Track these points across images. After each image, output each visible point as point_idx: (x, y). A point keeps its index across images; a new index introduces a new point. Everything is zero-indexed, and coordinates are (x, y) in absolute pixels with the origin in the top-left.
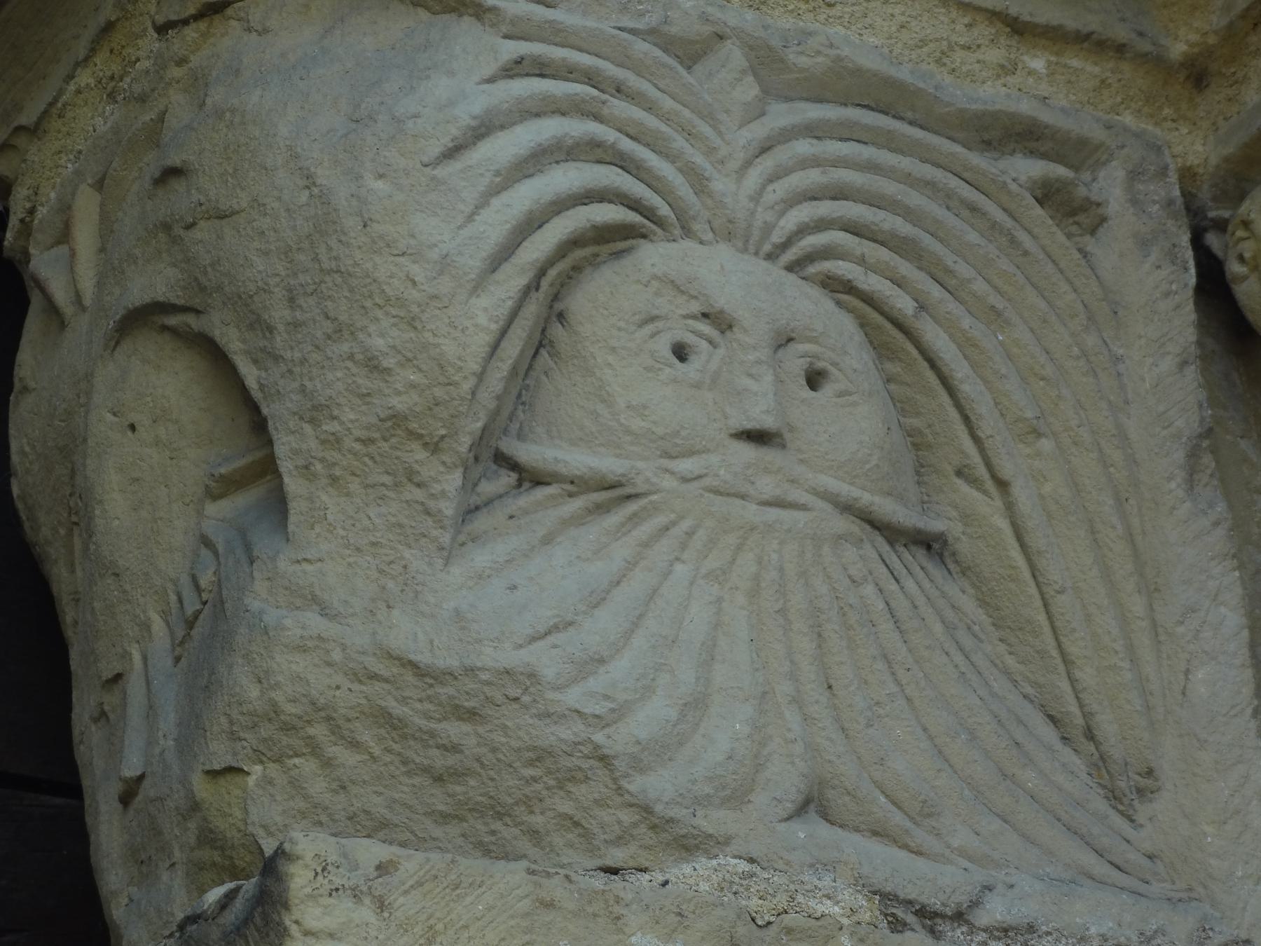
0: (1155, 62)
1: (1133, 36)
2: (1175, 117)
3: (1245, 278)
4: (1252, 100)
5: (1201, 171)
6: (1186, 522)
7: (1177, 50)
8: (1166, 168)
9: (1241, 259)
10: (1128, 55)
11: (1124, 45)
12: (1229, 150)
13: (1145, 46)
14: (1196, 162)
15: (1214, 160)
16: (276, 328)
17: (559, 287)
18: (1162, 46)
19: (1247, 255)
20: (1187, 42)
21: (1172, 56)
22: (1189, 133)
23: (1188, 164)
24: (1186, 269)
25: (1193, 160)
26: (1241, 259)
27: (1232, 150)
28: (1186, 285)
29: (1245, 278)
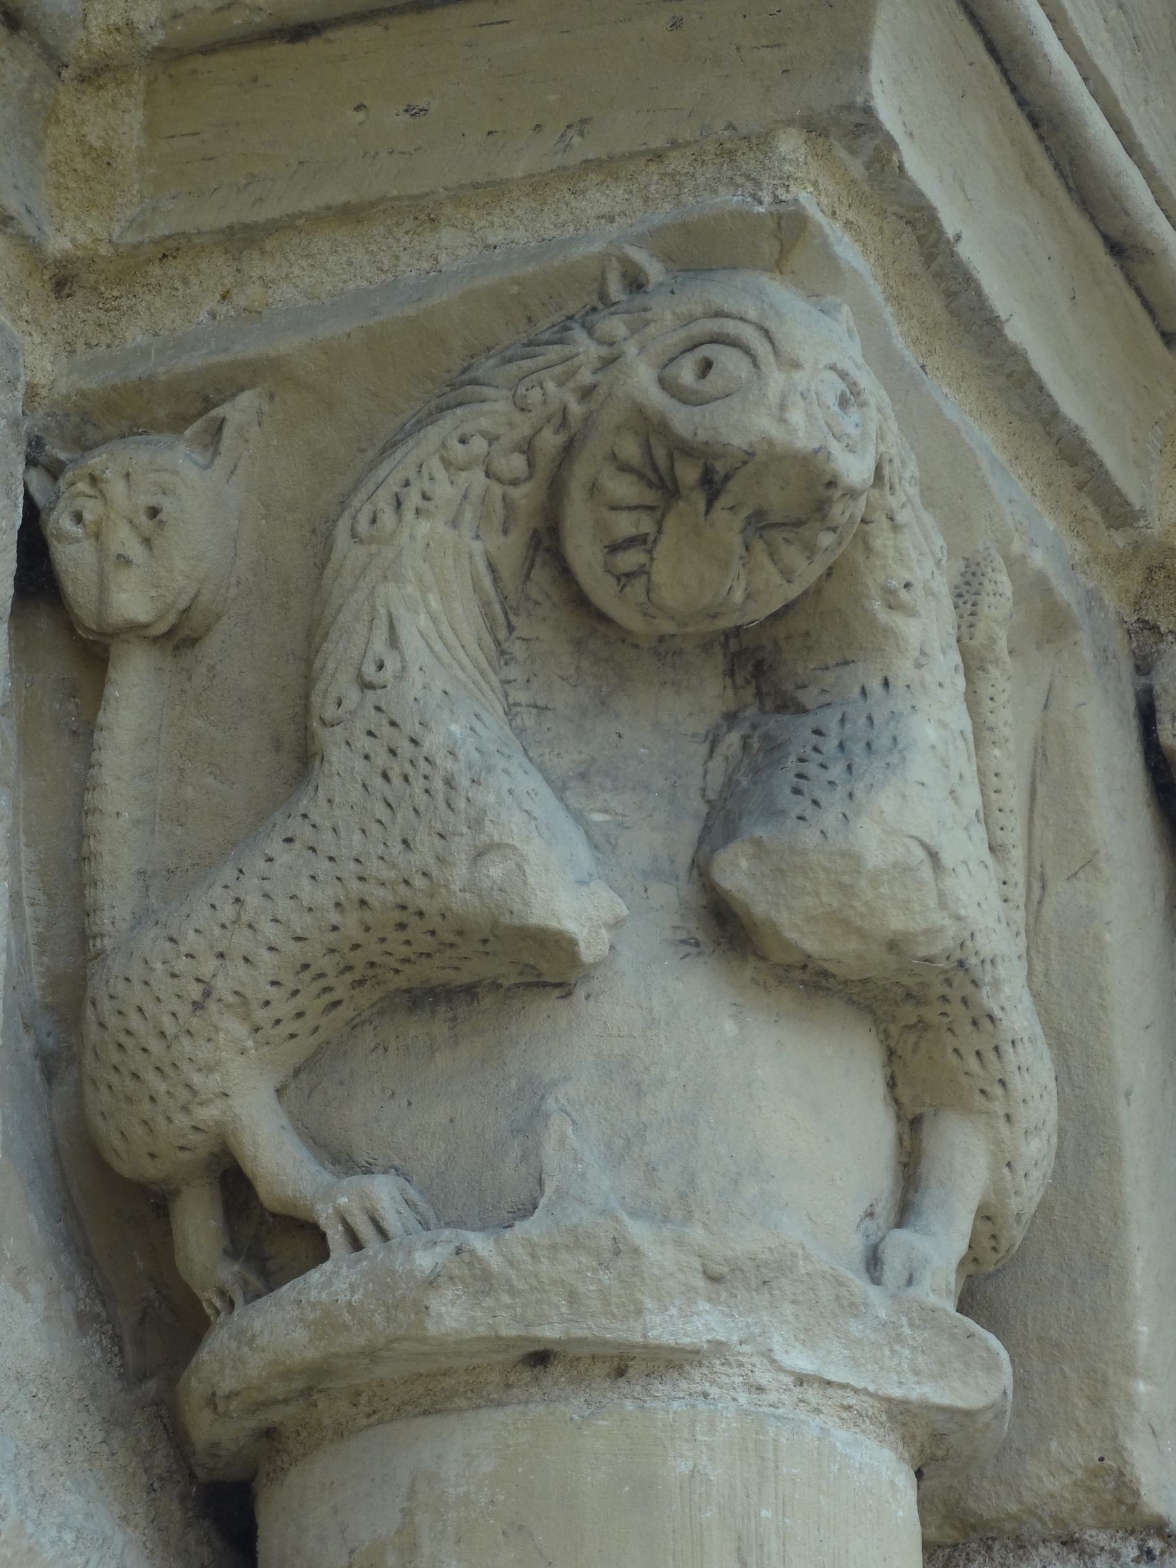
0: (31, 247)
1: (23, 211)
2: (29, 318)
3: (77, 540)
4: (134, 339)
5: (44, 393)
6: (439, 1275)
7: (58, 244)
8: (17, 378)
9: (78, 518)
10: (10, 230)
11: (12, 218)
12: (91, 384)
13: (29, 228)
14: (43, 381)
15: (63, 387)
16: (28, 434)
17: (945, 913)
18: (44, 233)
19: (87, 516)
20: (73, 240)
21: (50, 249)
22: (41, 344)
23: (35, 382)
24: (16, 506)
25: (41, 379)
26: (78, 518)
27: (93, 386)
28: (14, 526)
29: (77, 540)
